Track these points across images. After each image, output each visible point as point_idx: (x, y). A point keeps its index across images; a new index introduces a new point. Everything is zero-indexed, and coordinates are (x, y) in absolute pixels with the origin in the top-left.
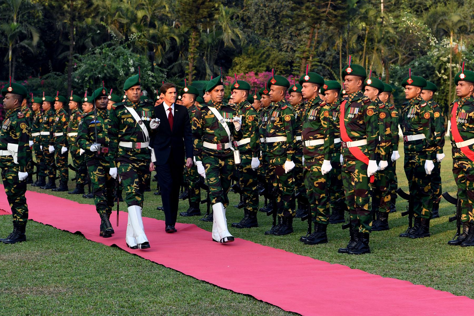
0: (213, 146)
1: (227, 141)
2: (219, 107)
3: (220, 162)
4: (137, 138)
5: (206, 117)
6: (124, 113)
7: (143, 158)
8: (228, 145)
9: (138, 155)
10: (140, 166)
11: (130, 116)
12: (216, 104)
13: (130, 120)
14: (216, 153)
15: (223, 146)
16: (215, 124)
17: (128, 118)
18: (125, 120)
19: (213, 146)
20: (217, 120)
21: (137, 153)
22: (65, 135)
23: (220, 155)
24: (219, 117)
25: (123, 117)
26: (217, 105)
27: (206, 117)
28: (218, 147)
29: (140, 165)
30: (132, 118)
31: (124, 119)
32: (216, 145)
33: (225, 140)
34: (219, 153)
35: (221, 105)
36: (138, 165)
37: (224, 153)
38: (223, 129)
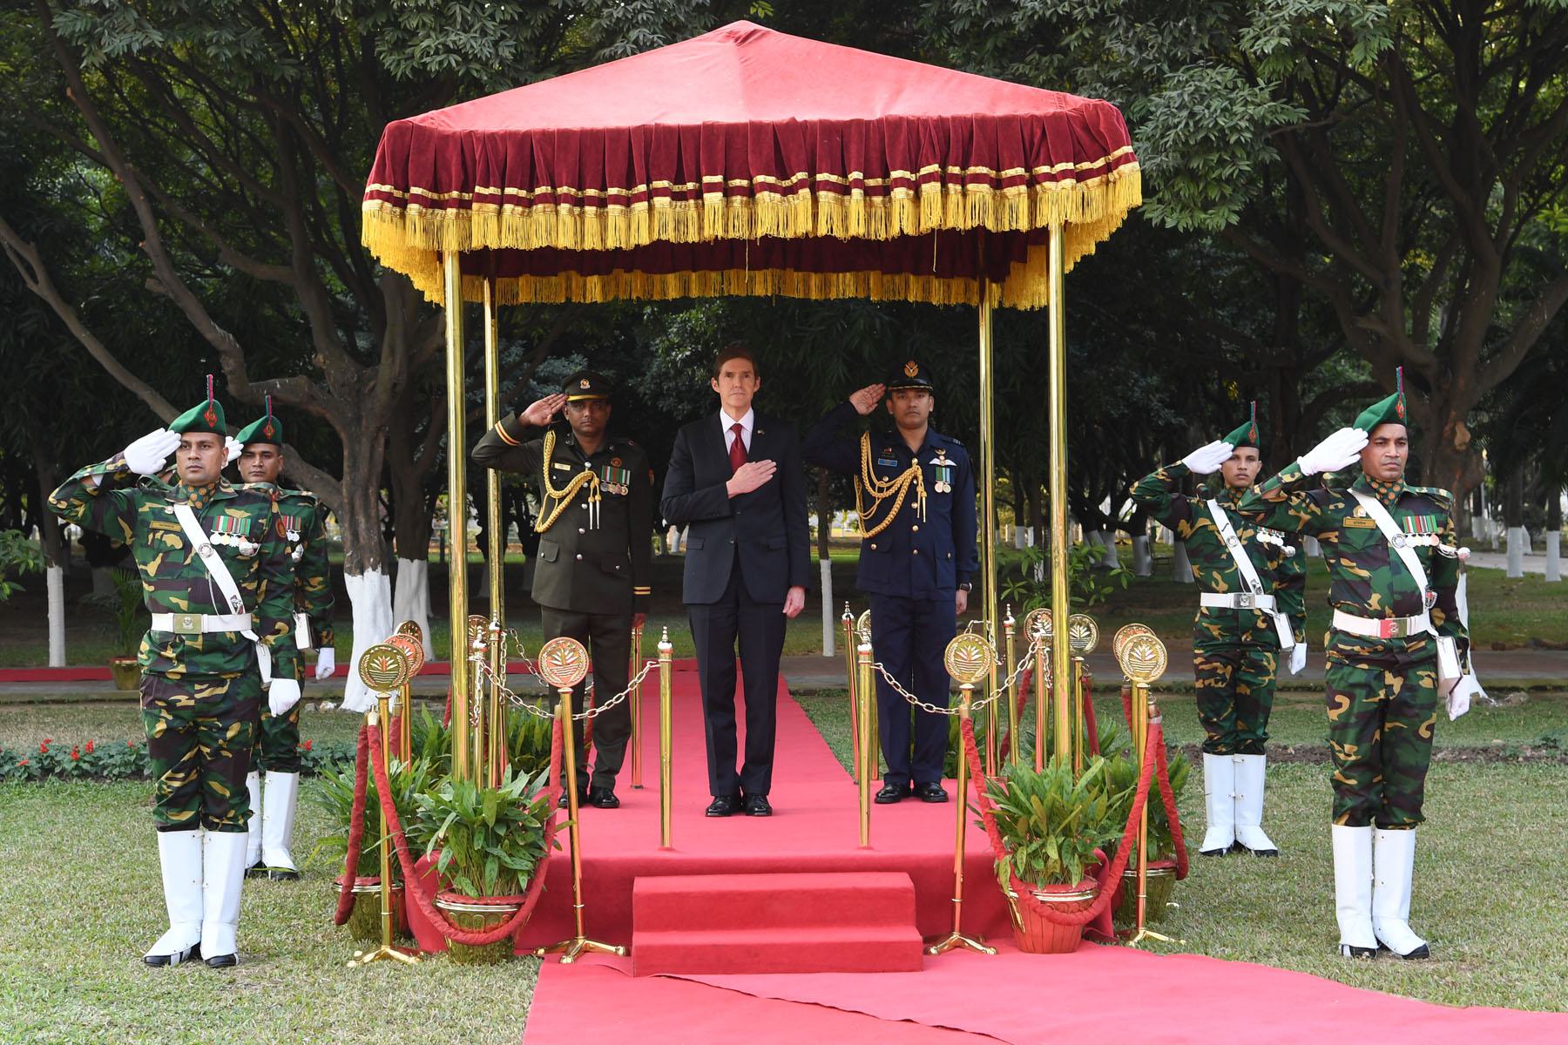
0: (1368, 628)
1: (1416, 609)
2: (1392, 496)
3: (1389, 678)
4: (191, 598)
5: (1348, 522)
6: (159, 515)
7: (212, 666)
8: (1420, 623)
9: (198, 658)
10: (197, 701)
11: (176, 528)
12: (1381, 485)
13: (173, 541)
14: (1376, 651)
15: (1403, 626)
16: (1376, 550)
17: (167, 532)
18: (158, 535)
19: (1368, 628)
20: (1384, 539)
21: (195, 651)
22: (726, 179)
23: (1387, 657)
24: (1387, 525)
25: (155, 525)
26: (1383, 491)
27: (1348, 522)
28: (1384, 628)
29: (198, 696)
30: (182, 535)
31: (155, 531)
32: (1376, 621)
33: (1407, 605)
34: (1388, 649)
35: (1397, 489)
36: (191, 697)
37: (1403, 650)
38: (1400, 567)
